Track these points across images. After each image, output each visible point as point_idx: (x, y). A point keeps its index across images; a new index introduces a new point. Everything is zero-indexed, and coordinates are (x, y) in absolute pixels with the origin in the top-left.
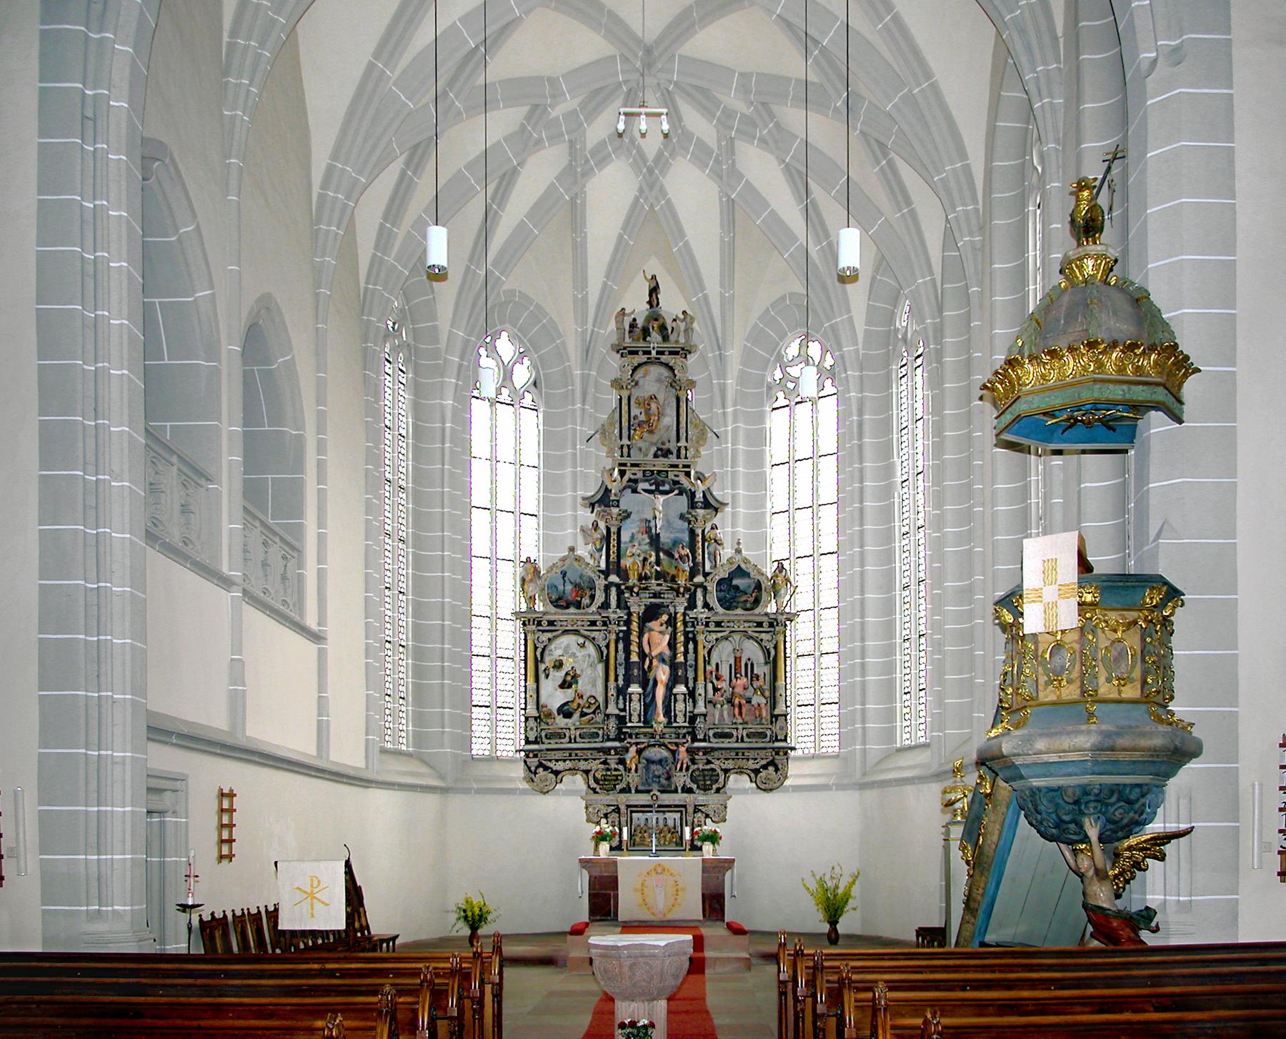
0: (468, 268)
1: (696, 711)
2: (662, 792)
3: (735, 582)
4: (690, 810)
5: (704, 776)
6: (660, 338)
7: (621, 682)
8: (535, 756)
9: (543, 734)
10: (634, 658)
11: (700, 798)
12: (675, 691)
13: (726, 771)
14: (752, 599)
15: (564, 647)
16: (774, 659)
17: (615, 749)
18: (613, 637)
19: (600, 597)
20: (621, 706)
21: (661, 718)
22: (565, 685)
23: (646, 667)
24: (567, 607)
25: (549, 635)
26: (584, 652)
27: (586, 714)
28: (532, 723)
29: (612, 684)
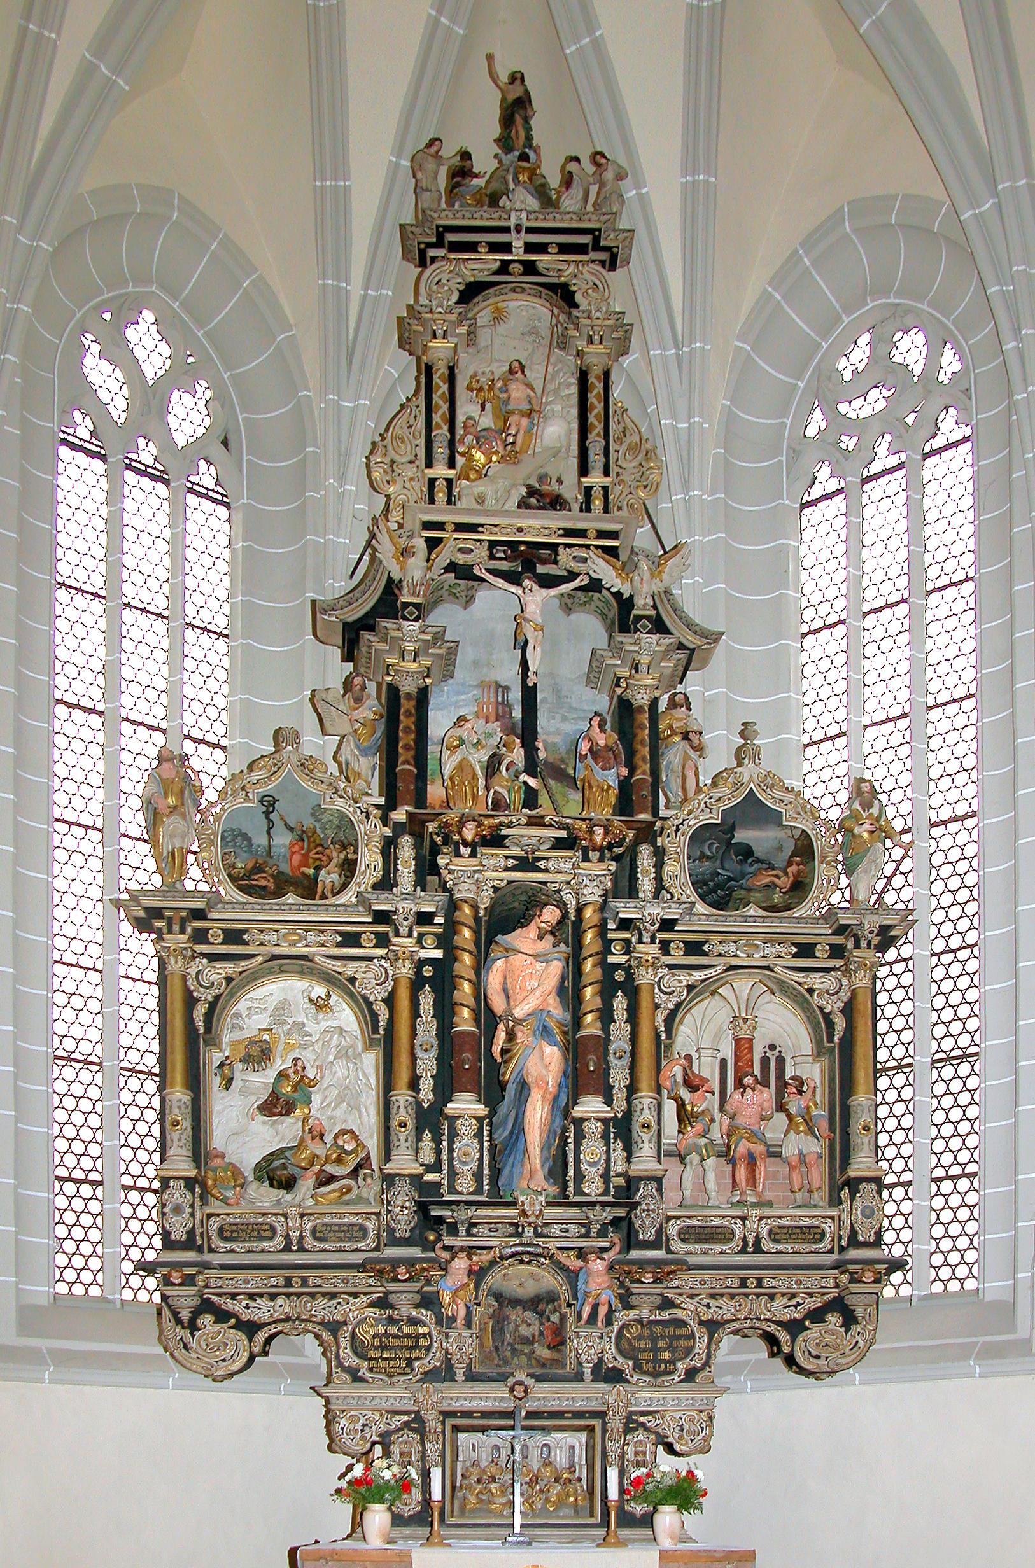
0: (24, 32)
1: (636, 1169)
2: (539, 1379)
3: (740, 836)
4: (616, 1423)
5: (654, 1339)
6: (533, 203)
7: (426, 1094)
8: (189, 1280)
9: (214, 1225)
10: (464, 1020)
11: (644, 1394)
12: (578, 1111)
13: (713, 1326)
14: (785, 882)
15: (268, 1005)
16: (846, 1043)
17: (410, 1262)
18: (406, 970)
19: (370, 860)
20: (428, 1157)
21: (540, 1180)
22: (275, 1106)
23: (496, 1050)
24: (279, 893)
25: (229, 968)
26: (326, 1022)
27: (331, 1179)
28: (178, 1195)
29: (402, 1097)
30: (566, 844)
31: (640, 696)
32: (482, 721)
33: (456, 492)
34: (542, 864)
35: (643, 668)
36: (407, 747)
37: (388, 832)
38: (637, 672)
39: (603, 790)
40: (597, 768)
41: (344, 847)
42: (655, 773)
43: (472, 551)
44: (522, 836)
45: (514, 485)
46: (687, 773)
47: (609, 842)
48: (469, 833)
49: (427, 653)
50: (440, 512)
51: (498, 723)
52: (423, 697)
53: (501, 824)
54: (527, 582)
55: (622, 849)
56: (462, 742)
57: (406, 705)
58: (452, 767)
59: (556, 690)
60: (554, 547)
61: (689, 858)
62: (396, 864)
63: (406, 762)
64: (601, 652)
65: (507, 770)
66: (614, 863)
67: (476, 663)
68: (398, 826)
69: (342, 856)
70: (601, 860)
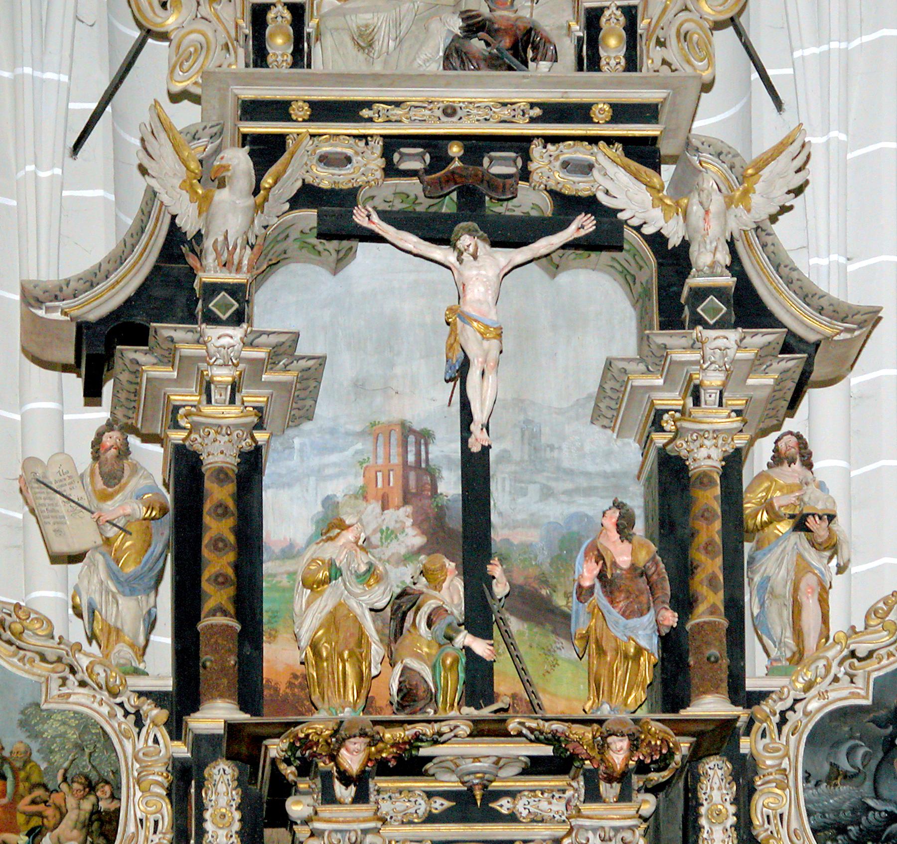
30: (558, 764)
31: (703, 452)
32: (374, 507)
33: (310, 28)
34: (504, 806)
35: (709, 397)
36: (220, 580)
37: (182, 750)
38: (697, 402)
39: (626, 657)
40: (613, 614)
41: (91, 787)
42: (734, 608)
43: (349, 160)
44: (463, 757)
45: (434, 10)
46: (802, 598)
47: (640, 763)
48: (352, 758)
49: (257, 382)
50: (278, 80)
51: (409, 509)
52: (251, 464)
53: (417, 738)
54: (466, 241)
55: (666, 775)
56: (335, 572)
57: (217, 494)
58: (316, 623)
59: (530, 435)
60: (521, 144)
61: (807, 779)
62: (200, 820)
63: (221, 610)
64: (621, 365)
65: (429, 624)
66: (651, 797)
67: (360, 386)
68: (200, 742)
69: (87, 805)
70: (624, 796)
